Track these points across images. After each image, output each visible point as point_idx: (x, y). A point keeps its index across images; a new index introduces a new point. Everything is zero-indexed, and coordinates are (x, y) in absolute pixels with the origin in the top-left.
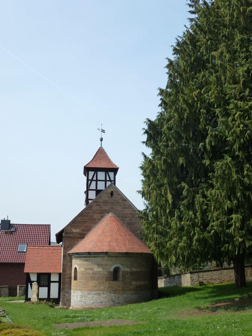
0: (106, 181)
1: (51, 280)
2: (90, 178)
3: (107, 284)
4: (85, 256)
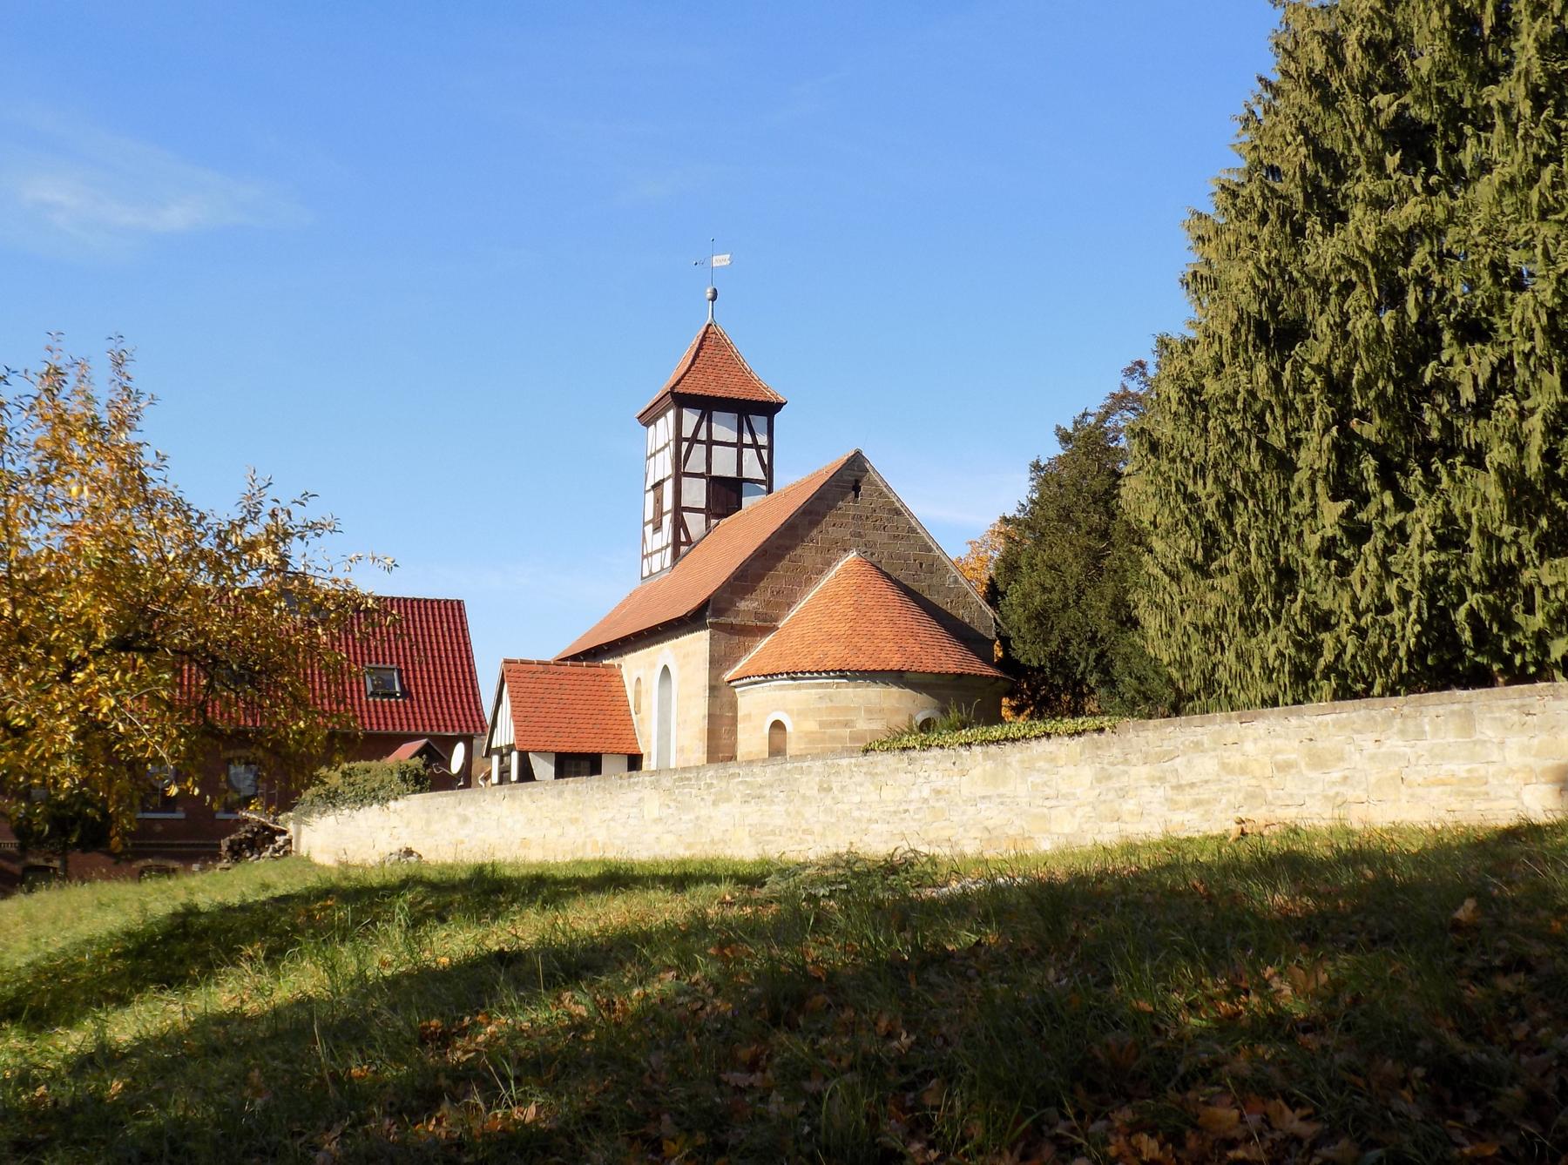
0: (740, 446)
2: (687, 432)
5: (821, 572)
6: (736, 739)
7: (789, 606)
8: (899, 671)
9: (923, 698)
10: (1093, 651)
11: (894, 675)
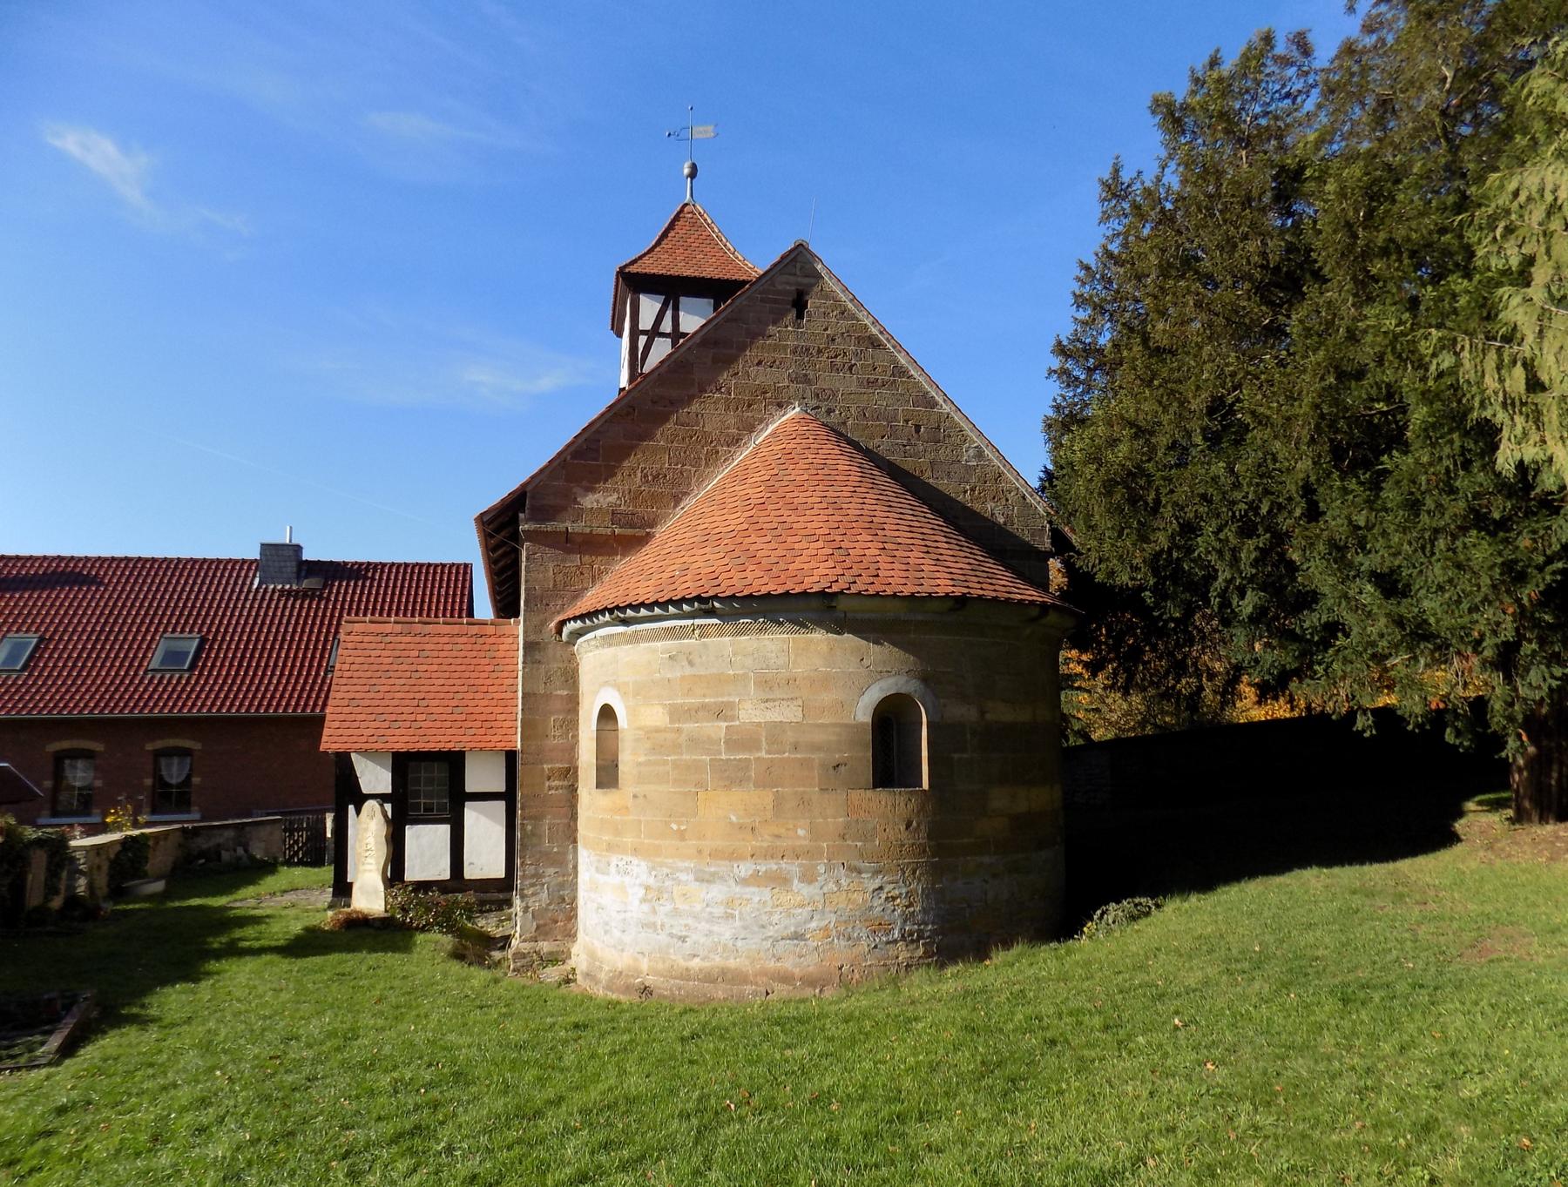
1: (467, 790)
3: (832, 813)
4: (667, 629)
5: (735, 441)
6: (576, 736)
7: (677, 500)
8: (822, 593)
9: (877, 653)
10: (1251, 543)
11: (814, 603)
